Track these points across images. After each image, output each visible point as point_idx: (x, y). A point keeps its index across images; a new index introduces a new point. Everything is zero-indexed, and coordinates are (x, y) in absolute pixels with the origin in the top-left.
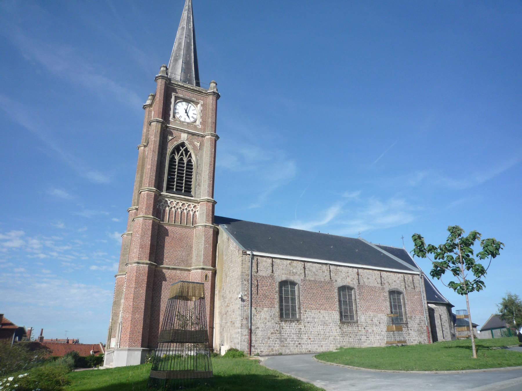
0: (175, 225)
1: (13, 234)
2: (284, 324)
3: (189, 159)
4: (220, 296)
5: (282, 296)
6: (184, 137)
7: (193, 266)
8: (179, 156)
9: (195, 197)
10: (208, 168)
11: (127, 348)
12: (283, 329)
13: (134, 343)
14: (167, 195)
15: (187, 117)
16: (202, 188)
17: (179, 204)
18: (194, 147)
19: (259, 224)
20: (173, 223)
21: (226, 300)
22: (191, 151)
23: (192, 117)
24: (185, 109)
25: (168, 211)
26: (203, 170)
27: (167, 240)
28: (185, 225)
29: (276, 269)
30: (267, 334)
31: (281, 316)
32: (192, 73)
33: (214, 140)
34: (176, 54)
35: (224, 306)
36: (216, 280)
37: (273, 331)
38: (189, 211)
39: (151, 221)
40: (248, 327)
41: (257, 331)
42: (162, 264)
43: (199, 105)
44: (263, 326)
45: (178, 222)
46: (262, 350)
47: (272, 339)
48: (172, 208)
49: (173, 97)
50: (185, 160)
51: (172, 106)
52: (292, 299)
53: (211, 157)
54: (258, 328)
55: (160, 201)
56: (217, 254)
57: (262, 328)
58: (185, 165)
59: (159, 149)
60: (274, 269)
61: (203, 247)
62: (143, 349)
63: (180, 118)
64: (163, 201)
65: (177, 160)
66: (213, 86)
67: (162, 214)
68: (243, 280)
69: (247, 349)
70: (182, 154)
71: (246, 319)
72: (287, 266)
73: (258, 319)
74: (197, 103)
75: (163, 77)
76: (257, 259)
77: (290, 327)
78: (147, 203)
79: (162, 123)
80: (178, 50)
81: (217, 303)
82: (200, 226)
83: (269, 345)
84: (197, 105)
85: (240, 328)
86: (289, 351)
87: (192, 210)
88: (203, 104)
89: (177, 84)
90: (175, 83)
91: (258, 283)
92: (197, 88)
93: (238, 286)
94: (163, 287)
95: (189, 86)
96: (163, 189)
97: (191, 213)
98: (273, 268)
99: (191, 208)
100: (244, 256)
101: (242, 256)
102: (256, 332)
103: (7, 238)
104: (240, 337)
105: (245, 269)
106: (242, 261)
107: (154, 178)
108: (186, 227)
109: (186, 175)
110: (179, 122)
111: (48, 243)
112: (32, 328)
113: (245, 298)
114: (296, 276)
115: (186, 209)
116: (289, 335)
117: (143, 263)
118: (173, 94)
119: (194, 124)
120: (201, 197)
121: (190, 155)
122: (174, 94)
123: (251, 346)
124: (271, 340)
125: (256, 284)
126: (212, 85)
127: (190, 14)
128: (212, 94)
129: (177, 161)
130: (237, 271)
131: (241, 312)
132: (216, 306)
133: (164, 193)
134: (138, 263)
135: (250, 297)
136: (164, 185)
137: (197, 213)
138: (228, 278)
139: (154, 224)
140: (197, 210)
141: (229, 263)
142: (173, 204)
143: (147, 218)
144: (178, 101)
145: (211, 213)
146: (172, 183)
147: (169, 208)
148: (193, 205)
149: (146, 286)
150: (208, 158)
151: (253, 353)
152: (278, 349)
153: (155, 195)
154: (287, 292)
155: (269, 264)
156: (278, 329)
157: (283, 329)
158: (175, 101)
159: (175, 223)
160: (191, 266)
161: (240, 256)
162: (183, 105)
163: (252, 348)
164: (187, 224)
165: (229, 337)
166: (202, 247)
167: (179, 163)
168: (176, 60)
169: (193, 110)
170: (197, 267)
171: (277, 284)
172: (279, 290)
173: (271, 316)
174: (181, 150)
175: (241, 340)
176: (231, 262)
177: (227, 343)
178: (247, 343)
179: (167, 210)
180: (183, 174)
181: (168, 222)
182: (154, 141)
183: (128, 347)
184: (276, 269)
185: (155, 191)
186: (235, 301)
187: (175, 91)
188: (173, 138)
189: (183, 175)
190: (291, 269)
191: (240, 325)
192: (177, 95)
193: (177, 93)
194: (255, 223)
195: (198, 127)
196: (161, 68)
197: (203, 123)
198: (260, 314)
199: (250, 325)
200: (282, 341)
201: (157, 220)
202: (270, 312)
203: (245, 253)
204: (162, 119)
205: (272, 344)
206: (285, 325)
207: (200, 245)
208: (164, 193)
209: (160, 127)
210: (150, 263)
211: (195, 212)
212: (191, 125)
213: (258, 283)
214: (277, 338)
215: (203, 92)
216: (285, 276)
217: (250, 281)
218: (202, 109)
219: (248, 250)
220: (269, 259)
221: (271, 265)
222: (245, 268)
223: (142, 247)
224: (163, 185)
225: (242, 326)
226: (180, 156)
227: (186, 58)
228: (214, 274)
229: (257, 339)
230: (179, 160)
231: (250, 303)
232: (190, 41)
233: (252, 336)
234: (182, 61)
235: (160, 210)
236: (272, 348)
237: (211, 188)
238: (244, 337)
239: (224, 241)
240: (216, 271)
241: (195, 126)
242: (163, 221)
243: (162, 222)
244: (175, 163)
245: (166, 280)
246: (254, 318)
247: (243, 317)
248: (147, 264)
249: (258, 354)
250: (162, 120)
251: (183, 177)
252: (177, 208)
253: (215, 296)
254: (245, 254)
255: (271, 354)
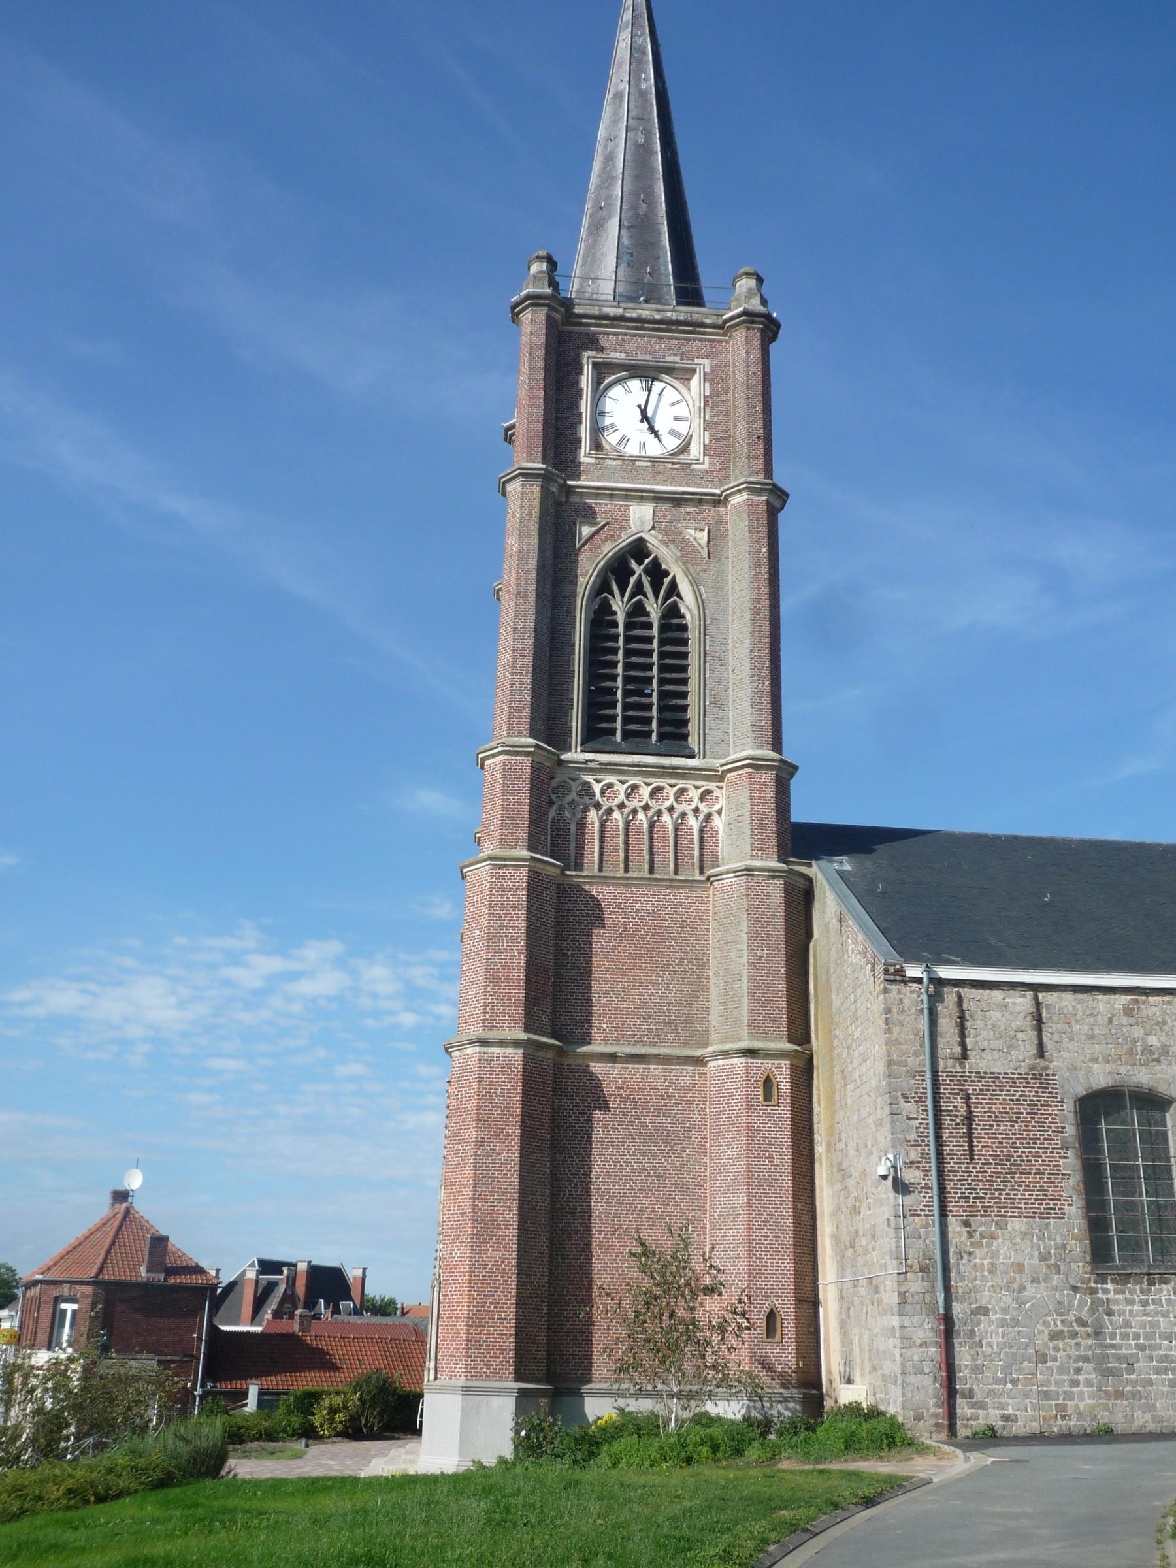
0: (628, 878)
1: (313, 952)
2: (1116, 1292)
3: (668, 602)
4: (832, 1165)
5: (1099, 1159)
6: (640, 516)
7: (712, 1045)
8: (626, 599)
9: (704, 757)
10: (747, 629)
11: (462, 1381)
12: (1110, 1313)
13: (488, 1365)
14: (587, 761)
15: (650, 438)
16: (731, 713)
17: (641, 791)
18: (686, 551)
19: (1014, 842)
20: (621, 873)
21: (851, 1183)
22: (675, 570)
23: (673, 432)
24: (639, 406)
25: (597, 825)
26: (730, 641)
27: (601, 940)
28: (672, 875)
29: (1056, 1037)
30: (1031, 1337)
31: (1100, 1254)
32: (661, 260)
33: (763, 509)
34: (597, 201)
35: (844, 1209)
36: (815, 1099)
37: (1059, 1323)
38: (683, 815)
39: (524, 872)
40: (931, 1309)
41: (979, 1324)
42: (586, 1039)
43: (695, 381)
44: (1009, 1300)
45: (640, 868)
46: (1010, 1411)
47: (1058, 1364)
48: (610, 811)
49: (586, 367)
50: (654, 609)
51: (585, 406)
52: (1149, 1171)
53: (758, 579)
54: (984, 1311)
55: (564, 789)
56: (811, 987)
57: (1006, 1310)
58: (655, 631)
59: (538, 581)
60: (1045, 1040)
61: (745, 960)
62: (520, 1390)
63: (621, 448)
64: (575, 786)
65: (619, 613)
66: (744, 289)
67: (573, 839)
68: (895, 1096)
69: (937, 1406)
70: (639, 589)
71: (922, 1270)
72: (1115, 1019)
73: (983, 1270)
74: (684, 374)
75: (535, 300)
76: (960, 999)
77: (1145, 1304)
78: (505, 800)
79: (546, 478)
80: (604, 183)
81: (825, 1194)
82: (728, 872)
83: (1045, 1389)
84: (689, 379)
85: (896, 1310)
86: (1148, 1416)
87: (696, 811)
88: (712, 371)
89: (597, 312)
90: (589, 312)
91: (969, 1107)
92: (683, 313)
93: (881, 1124)
94: (597, 1134)
95: (647, 311)
96: (571, 737)
97: (693, 823)
98: (1044, 1033)
99: (690, 801)
100: (895, 988)
101: (886, 991)
102: (972, 1331)
103: (293, 966)
104: (897, 1352)
105: (904, 1047)
106: (888, 1011)
107: (528, 699)
108: (671, 883)
109: (663, 668)
110: (619, 462)
111: (420, 974)
112: (364, 1270)
113: (910, 1176)
114: (1165, 1067)
115: (671, 809)
116: (1141, 1341)
117: (501, 1043)
118: (587, 358)
119: (681, 457)
120: (731, 752)
121: (673, 586)
122: (588, 358)
123: (951, 1392)
124: (1051, 1368)
125: (963, 1111)
126: (741, 286)
127: (643, 34)
128: (743, 322)
129: (621, 619)
130: (872, 1058)
131: (898, 1242)
132: (822, 1206)
133: (575, 755)
134: (483, 1042)
135: (934, 1172)
136: (574, 724)
137: (718, 822)
138: (850, 1087)
139: (536, 884)
140: (717, 807)
141: (849, 1023)
142: (616, 793)
143: (505, 859)
144: (607, 380)
145: (771, 814)
146: (608, 712)
147: (601, 812)
148: (697, 787)
149: (518, 1132)
150: (745, 584)
151: (966, 1426)
152: (1093, 1407)
153: (536, 769)
154: (1122, 1142)
155: (1022, 1016)
156: (1085, 1314)
157: (1110, 1313)
158: (598, 381)
159: (626, 870)
160: (706, 1045)
161: (878, 989)
162: (629, 391)
163: (959, 1401)
164: (676, 872)
165: (867, 1348)
166: (741, 960)
167: (629, 626)
168: (598, 226)
169: (672, 405)
170: (727, 1046)
171: (1069, 1106)
172: (1078, 1136)
173: (1044, 1257)
174: (633, 573)
175: (903, 1365)
176: (855, 1018)
177: (863, 1375)
178: (935, 1380)
179: (592, 823)
180: (649, 667)
181: (601, 870)
182: (520, 552)
183: (463, 1377)
184: (1056, 1037)
185: (532, 749)
186: (877, 1188)
187: (592, 343)
188: (597, 532)
189: (648, 673)
190: (1138, 1032)
191: (896, 1299)
192: (601, 357)
193: (600, 349)
194: (997, 838)
195: (697, 466)
196: (531, 268)
197: (718, 447)
198: (989, 1245)
199: (941, 1297)
200: (1111, 1372)
201: (548, 868)
202: (1039, 1239)
203: (896, 977)
204: (543, 463)
205: (1056, 1383)
206: (1120, 1297)
207: (733, 954)
208: (575, 756)
209: (539, 495)
210: (529, 1041)
211: (708, 817)
212: (670, 466)
213: (969, 1107)
214: (1085, 1359)
215: (708, 321)
216: (1108, 1068)
217: (929, 1102)
218: (707, 393)
219: (917, 959)
220: (1017, 993)
221: (1029, 1023)
222: (900, 1044)
223: (494, 977)
224: (571, 721)
225: (903, 1303)
226: (632, 596)
227: (634, 208)
228: (804, 1073)
229: (979, 1362)
230: (629, 615)
231: (936, 1199)
232: (646, 138)
233: (957, 1348)
234: (618, 223)
235: (566, 824)
236: (1060, 1402)
237: (767, 711)
238: (916, 1354)
239: (831, 926)
240: (810, 1059)
241: (686, 466)
242: (579, 866)
243: (574, 873)
244: (613, 630)
245: (605, 1107)
246: (961, 1268)
247: (909, 1262)
248: (516, 1044)
249: (992, 1429)
250: (544, 466)
251: (649, 680)
252: (631, 807)
253: (817, 1166)
254: (898, 978)
255: (1055, 1429)
